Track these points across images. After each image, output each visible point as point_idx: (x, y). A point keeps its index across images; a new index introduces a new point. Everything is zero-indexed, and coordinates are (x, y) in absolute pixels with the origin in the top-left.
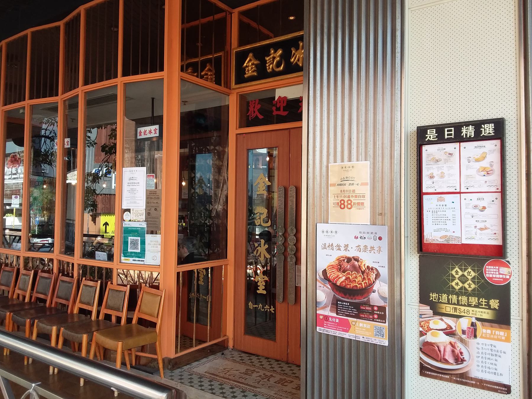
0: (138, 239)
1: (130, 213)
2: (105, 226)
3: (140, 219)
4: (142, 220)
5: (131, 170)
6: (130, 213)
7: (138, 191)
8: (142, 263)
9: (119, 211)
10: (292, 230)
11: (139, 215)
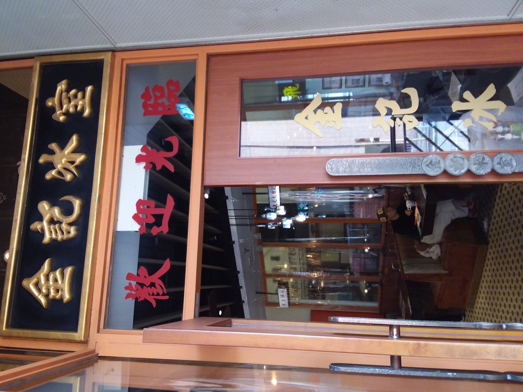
10: (431, 163)
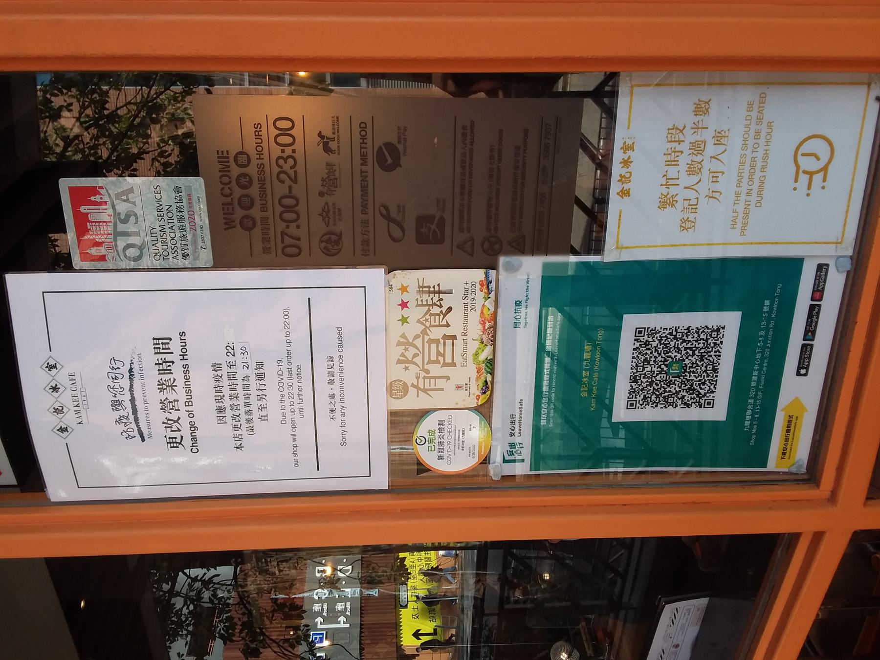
0: (639, 331)
1: (423, 414)
2: (420, 637)
3: (474, 318)
4: (480, 295)
5: (54, 420)
6: (423, 414)
7: (230, 350)
8: (835, 284)
9: (408, 513)
11: (437, 333)
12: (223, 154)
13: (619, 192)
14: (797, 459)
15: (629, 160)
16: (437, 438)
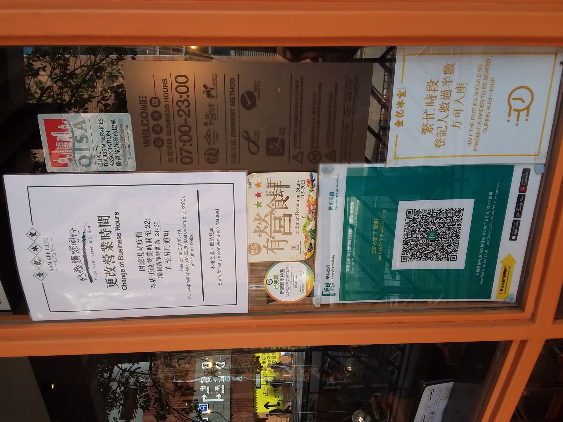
0: (409, 212)
1: (270, 265)
2: (269, 407)
3: (303, 203)
4: (307, 189)
5: (35, 269)
6: (270, 265)
7: (147, 224)
8: (534, 182)
9: (261, 328)
11: (280, 213)
12: (142, 99)
13: (396, 123)
14: (510, 293)
15: (403, 103)
16: (279, 280)
